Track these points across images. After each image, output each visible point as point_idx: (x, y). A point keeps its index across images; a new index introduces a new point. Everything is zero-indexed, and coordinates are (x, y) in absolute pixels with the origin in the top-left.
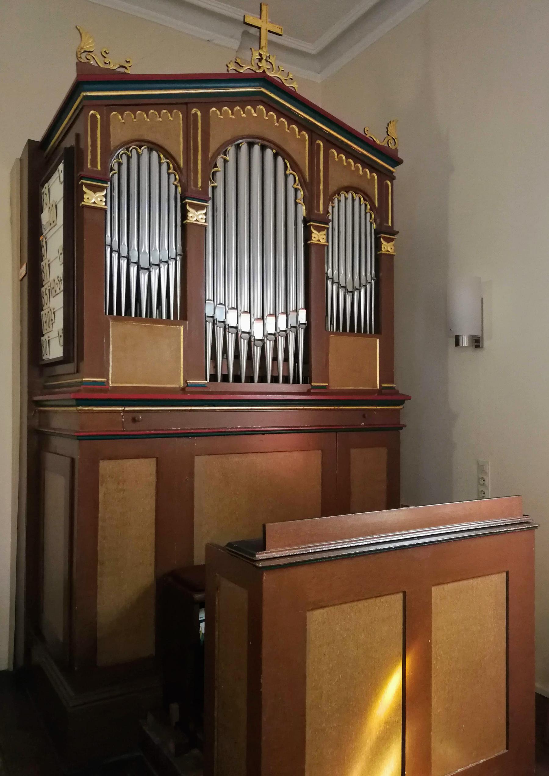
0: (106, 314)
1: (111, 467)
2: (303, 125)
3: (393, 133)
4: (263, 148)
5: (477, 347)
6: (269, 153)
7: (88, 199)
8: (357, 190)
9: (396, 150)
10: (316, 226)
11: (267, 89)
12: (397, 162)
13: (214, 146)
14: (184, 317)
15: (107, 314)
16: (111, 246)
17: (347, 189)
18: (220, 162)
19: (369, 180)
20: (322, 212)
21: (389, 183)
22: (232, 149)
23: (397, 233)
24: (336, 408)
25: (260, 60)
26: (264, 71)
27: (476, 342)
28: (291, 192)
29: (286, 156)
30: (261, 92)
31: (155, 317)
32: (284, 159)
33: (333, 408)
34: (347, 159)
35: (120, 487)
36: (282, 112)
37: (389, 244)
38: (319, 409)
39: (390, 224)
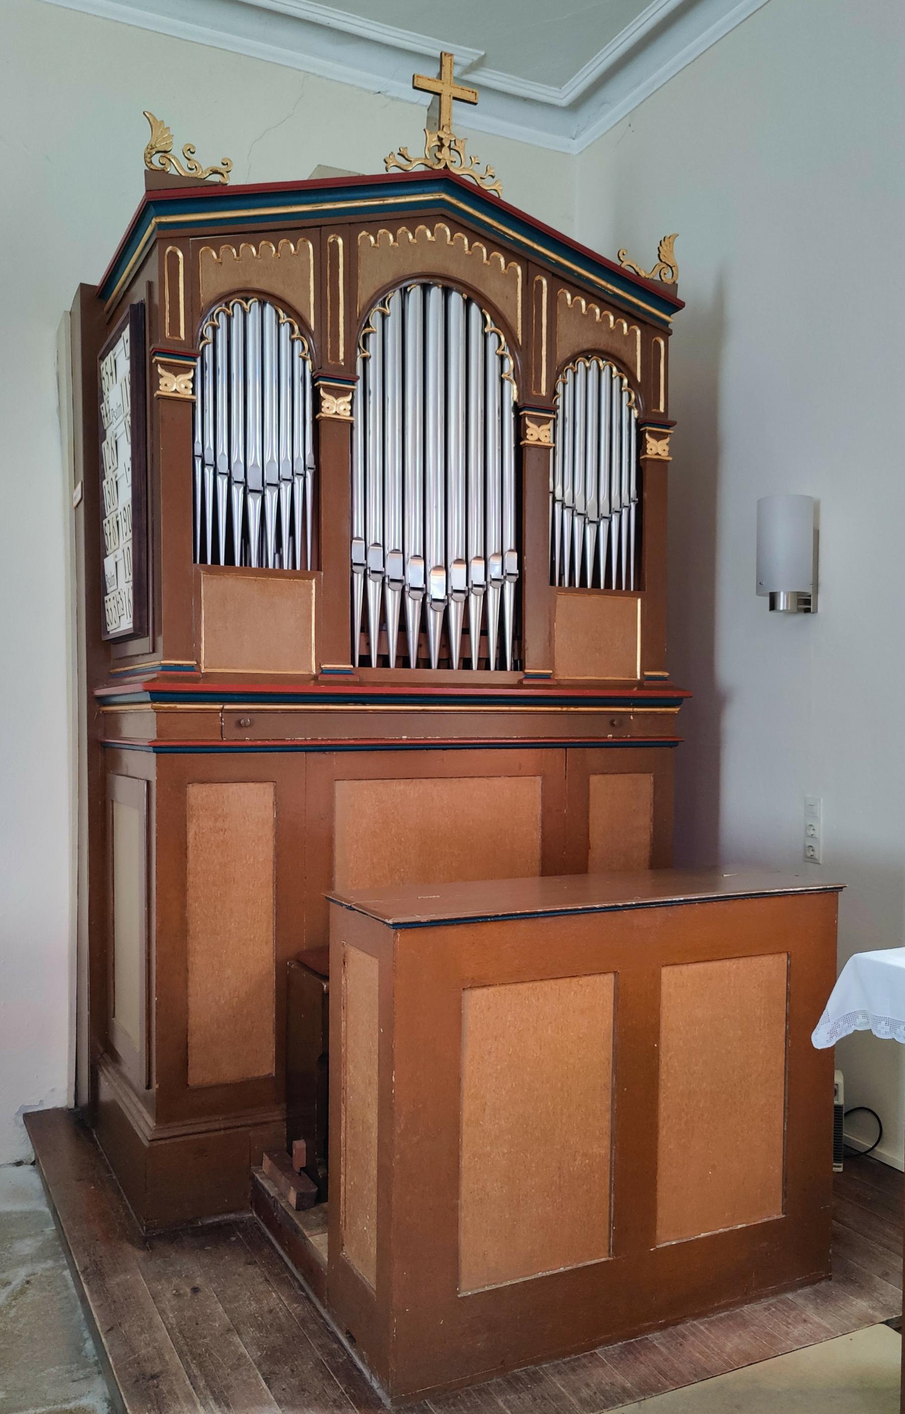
2: (513, 252)
3: (680, 255)
4: (446, 292)
5: (807, 611)
6: (456, 300)
9: (675, 285)
11: (451, 195)
12: (674, 306)
13: (364, 294)
17: (587, 354)
18: (375, 319)
19: (625, 337)
20: (544, 393)
21: (662, 343)
22: (395, 298)
24: (565, 709)
25: (441, 147)
26: (446, 167)
27: (805, 604)
29: (486, 304)
30: (442, 200)
31: (285, 568)
32: (481, 309)
33: (559, 709)
34: (587, 304)
35: (219, 824)
36: (477, 232)
39: (662, 409)
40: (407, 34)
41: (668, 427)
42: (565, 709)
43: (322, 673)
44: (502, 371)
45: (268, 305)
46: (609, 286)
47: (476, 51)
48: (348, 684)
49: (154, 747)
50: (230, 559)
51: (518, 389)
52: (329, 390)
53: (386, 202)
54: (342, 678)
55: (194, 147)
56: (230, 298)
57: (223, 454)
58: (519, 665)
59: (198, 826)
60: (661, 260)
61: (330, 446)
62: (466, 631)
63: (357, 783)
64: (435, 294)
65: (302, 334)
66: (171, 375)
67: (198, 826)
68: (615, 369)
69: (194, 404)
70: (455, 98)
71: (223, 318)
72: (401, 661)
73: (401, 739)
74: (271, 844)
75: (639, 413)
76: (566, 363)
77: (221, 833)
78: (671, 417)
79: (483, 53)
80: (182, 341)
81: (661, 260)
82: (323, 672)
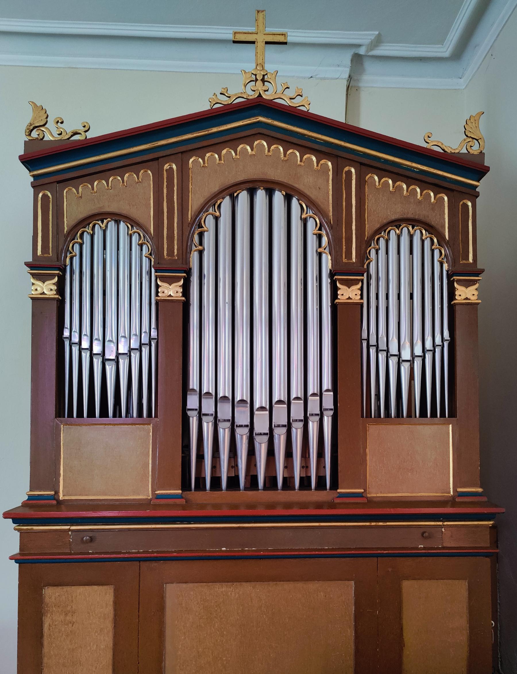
0: (362, 416)
1: (57, 594)
2: (322, 152)
4: (270, 193)
6: (278, 197)
7: (342, 295)
8: (414, 222)
9: (482, 154)
10: (342, 279)
13: (194, 202)
14: (453, 414)
16: (368, 340)
17: (397, 223)
18: (210, 222)
19: (432, 204)
20: (354, 260)
21: (470, 204)
22: (226, 203)
24: (373, 524)
28: (312, 240)
30: (259, 122)
32: (298, 200)
33: (368, 524)
34: (394, 182)
36: (289, 141)
37: (46, 283)
38: (345, 526)
39: (471, 260)
40: (326, 33)
44: (320, 246)
45: (122, 222)
46: (414, 165)
47: (372, 32)
51: (331, 259)
52: (459, 282)
53: (210, 132)
55: (61, 118)
58: (335, 485)
59: (52, 619)
60: (467, 136)
61: (175, 324)
63: (184, 585)
64: (261, 195)
65: (439, 245)
66: (166, 285)
67: (52, 619)
68: (424, 232)
69: (362, 305)
70: (267, 43)
71: (87, 238)
74: (111, 635)
75: (448, 266)
76: (378, 231)
77: (70, 625)
78: (479, 266)
79: (377, 33)
81: (467, 136)
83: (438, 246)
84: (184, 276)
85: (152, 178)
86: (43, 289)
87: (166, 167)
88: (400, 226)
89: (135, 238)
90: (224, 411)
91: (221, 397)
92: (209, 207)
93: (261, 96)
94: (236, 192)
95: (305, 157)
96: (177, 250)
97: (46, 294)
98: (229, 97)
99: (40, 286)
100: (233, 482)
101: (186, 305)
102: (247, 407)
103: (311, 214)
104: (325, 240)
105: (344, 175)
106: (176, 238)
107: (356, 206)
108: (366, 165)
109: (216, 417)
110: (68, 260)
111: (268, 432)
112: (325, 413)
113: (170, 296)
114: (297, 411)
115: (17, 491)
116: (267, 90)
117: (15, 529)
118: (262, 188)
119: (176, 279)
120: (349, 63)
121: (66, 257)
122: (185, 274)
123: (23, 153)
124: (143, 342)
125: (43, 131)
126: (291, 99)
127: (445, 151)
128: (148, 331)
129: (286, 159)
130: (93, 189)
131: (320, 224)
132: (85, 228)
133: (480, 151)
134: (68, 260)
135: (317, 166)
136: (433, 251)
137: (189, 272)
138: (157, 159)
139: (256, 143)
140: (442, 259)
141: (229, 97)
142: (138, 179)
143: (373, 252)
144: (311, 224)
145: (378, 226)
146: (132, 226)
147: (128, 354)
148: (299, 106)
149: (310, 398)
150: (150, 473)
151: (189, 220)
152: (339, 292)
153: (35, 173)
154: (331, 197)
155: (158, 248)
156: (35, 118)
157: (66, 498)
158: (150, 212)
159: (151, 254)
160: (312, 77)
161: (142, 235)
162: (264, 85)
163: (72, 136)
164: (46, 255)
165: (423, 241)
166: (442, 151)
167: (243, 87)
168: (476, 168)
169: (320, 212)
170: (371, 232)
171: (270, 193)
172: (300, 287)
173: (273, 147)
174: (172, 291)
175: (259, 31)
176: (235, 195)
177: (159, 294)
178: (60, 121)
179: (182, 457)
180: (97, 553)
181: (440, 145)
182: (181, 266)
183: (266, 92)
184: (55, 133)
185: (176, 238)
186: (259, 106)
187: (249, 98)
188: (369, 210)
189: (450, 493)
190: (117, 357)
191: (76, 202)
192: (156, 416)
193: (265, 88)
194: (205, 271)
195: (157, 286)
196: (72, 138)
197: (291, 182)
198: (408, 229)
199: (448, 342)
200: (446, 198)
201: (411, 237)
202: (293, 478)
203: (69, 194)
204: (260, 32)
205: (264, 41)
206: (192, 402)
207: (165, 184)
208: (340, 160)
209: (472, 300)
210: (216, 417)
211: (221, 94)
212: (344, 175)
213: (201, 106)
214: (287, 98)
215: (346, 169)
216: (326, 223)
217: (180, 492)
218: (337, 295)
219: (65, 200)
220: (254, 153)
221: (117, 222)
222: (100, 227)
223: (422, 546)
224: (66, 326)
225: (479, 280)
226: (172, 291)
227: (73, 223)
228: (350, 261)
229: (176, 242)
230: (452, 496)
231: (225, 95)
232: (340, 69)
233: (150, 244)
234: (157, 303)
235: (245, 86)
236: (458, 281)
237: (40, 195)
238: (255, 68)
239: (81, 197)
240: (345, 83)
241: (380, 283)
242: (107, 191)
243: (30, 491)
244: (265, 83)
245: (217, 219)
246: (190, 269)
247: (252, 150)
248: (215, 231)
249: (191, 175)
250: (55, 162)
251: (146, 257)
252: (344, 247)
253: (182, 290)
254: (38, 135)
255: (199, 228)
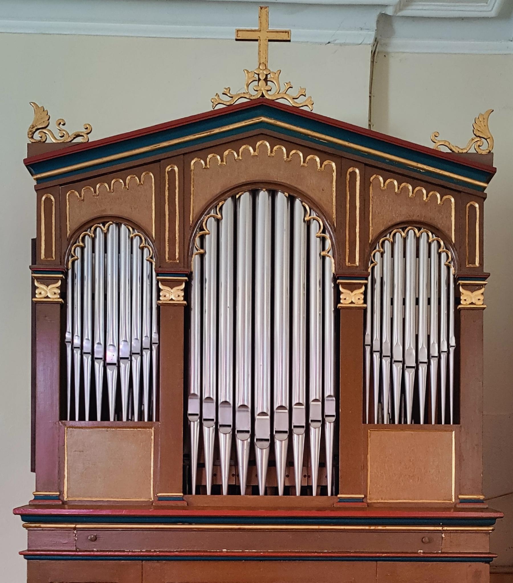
0: (364, 422)
2: (326, 152)
3: (495, 127)
4: (273, 195)
6: (281, 198)
7: (345, 299)
8: (419, 224)
13: (195, 206)
14: (457, 421)
15: (409, 422)
17: (403, 225)
18: (211, 225)
19: (439, 206)
20: (357, 264)
21: (477, 205)
23: (488, 275)
24: (372, 528)
26: (263, 96)
30: (261, 122)
31: (385, 423)
32: (302, 202)
33: (367, 528)
34: (399, 184)
36: (292, 141)
37: (50, 287)
38: (344, 530)
39: (477, 264)
41: (484, 279)
42: (372, 528)
43: (458, 501)
44: (324, 249)
45: (123, 225)
46: (420, 165)
48: (482, 510)
49: (25, 555)
50: (427, 420)
51: (335, 263)
52: (464, 286)
54: (172, 503)
56: (91, 224)
57: (434, 343)
58: (336, 491)
61: (176, 326)
62: (290, 463)
64: (263, 197)
65: (446, 249)
66: (168, 289)
68: (430, 234)
69: (365, 310)
70: (269, 41)
71: (88, 241)
72: (250, 490)
73: (222, 552)
75: (455, 270)
76: (383, 233)
80: (476, 268)
81: (475, 135)
82: (161, 499)
83: (445, 249)
84: (186, 280)
85: (153, 180)
86: (47, 292)
87: (168, 169)
88: (406, 228)
89: (136, 241)
90: (225, 417)
91: (223, 402)
92: (211, 209)
93: (264, 96)
94: (238, 194)
95: (308, 158)
96: (179, 253)
97: (49, 298)
98: (232, 97)
99: (44, 290)
100: (234, 489)
101: (188, 309)
102: (248, 411)
103: (315, 216)
104: (328, 243)
105: (348, 176)
106: (177, 241)
107: (360, 208)
108: (371, 166)
109: (217, 423)
110: (70, 263)
111: (269, 438)
112: (327, 419)
113: (172, 300)
114: (299, 418)
115: (25, 489)
116: (270, 90)
117: (24, 526)
118: (264, 190)
119: (178, 283)
120: (374, 26)
121: (68, 261)
122: (186, 278)
123: (26, 157)
124: (144, 346)
125: (45, 133)
126: (294, 99)
127: (453, 151)
128: (149, 335)
129: (289, 159)
130: (95, 192)
131: (324, 226)
132: (86, 231)
133: (488, 151)
134: (70, 263)
135: (321, 166)
136: (440, 254)
137: (190, 275)
138: (159, 161)
139: (258, 143)
140: (449, 263)
141: (232, 97)
142: (140, 181)
143: (378, 255)
144: (314, 226)
145: (382, 229)
146: (133, 229)
147: (130, 359)
148: (302, 106)
149: (312, 403)
150: (152, 476)
151: (191, 222)
152: (342, 296)
153: (39, 176)
154: (334, 199)
155: (159, 251)
156: (36, 120)
157: (70, 499)
158: (152, 215)
159: (152, 258)
160: (329, 43)
161: (143, 238)
162: (267, 85)
163: (74, 138)
164: (49, 259)
165: (430, 244)
166: (450, 151)
167: (246, 87)
168: (482, 169)
169: (323, 214)
170: (376, 234)
171: (273, 195)
172: (303, 292)
173: (275, 148)
174: (173, 295)
175: (262, 28)
176: (237, 196)
177: (161, 298)
178: (62, 123)
179: (183, 465)
180: (101, 551)
181: (447, 144)
182: (182, 269)
183: (269, 92)
184: (58, 135)
185: (177, 241)
186: (262, 106)
187: (251, 98)
188: (374, 212)
189: (451, 500)
190: (119, 362)
191: (78, 205)
192: (158, 419)
193: (267, 88)
194: (207, 275)
195: (159, 290)
196: (74, 141)
197: (293, 184)
198: (415, 232)
199: (454, 348)
200: (453, 200)
201: (418, 240)
202: (294, 487)
203: (71, 196)
204: (264, 30)
205: (268, 39)
206: (193, 407)
207: (167, 186)
208: (344, 160)
209: (477, 305)
210: (217, 423)
211: (223, 94)
212: (348, 176)
213: (204, 107)
214: (290, 98)
215: (351, 170)
216: (330, 225)
217: (182, 494)
218: (340, 299)
219: (68, 203)
220: (256, 154)
221: (119, 225)
222: (102, 230)
223: (422, 551)
224: (68, 330)
225: (485, 284)
226: (173, 295)
227: (75, 227)
228: (353, 265)
229: (177, 245)
230: (454, 503)
231: (227, 95)
232: (364, 32)
233: (152, 248)
234: (158, 308)
235: (248, 86)
236: (464, 285)
237: (44, 198)
238: (258, 67)
239: (83, 200)
240: (370, 49)
241: (385, 288)
242: (109, 194)
243: (37, 491)
244: (268, 82)
245: (218, 221)
246: (192, 273)
247: (255, 151)
248: (217, 232)
249: (192, 177)
250: (59, 166)
251: (147, 260)
252: (347, 250)
253: (183, 294)
254: (41, 137)
255: (200, 231)
